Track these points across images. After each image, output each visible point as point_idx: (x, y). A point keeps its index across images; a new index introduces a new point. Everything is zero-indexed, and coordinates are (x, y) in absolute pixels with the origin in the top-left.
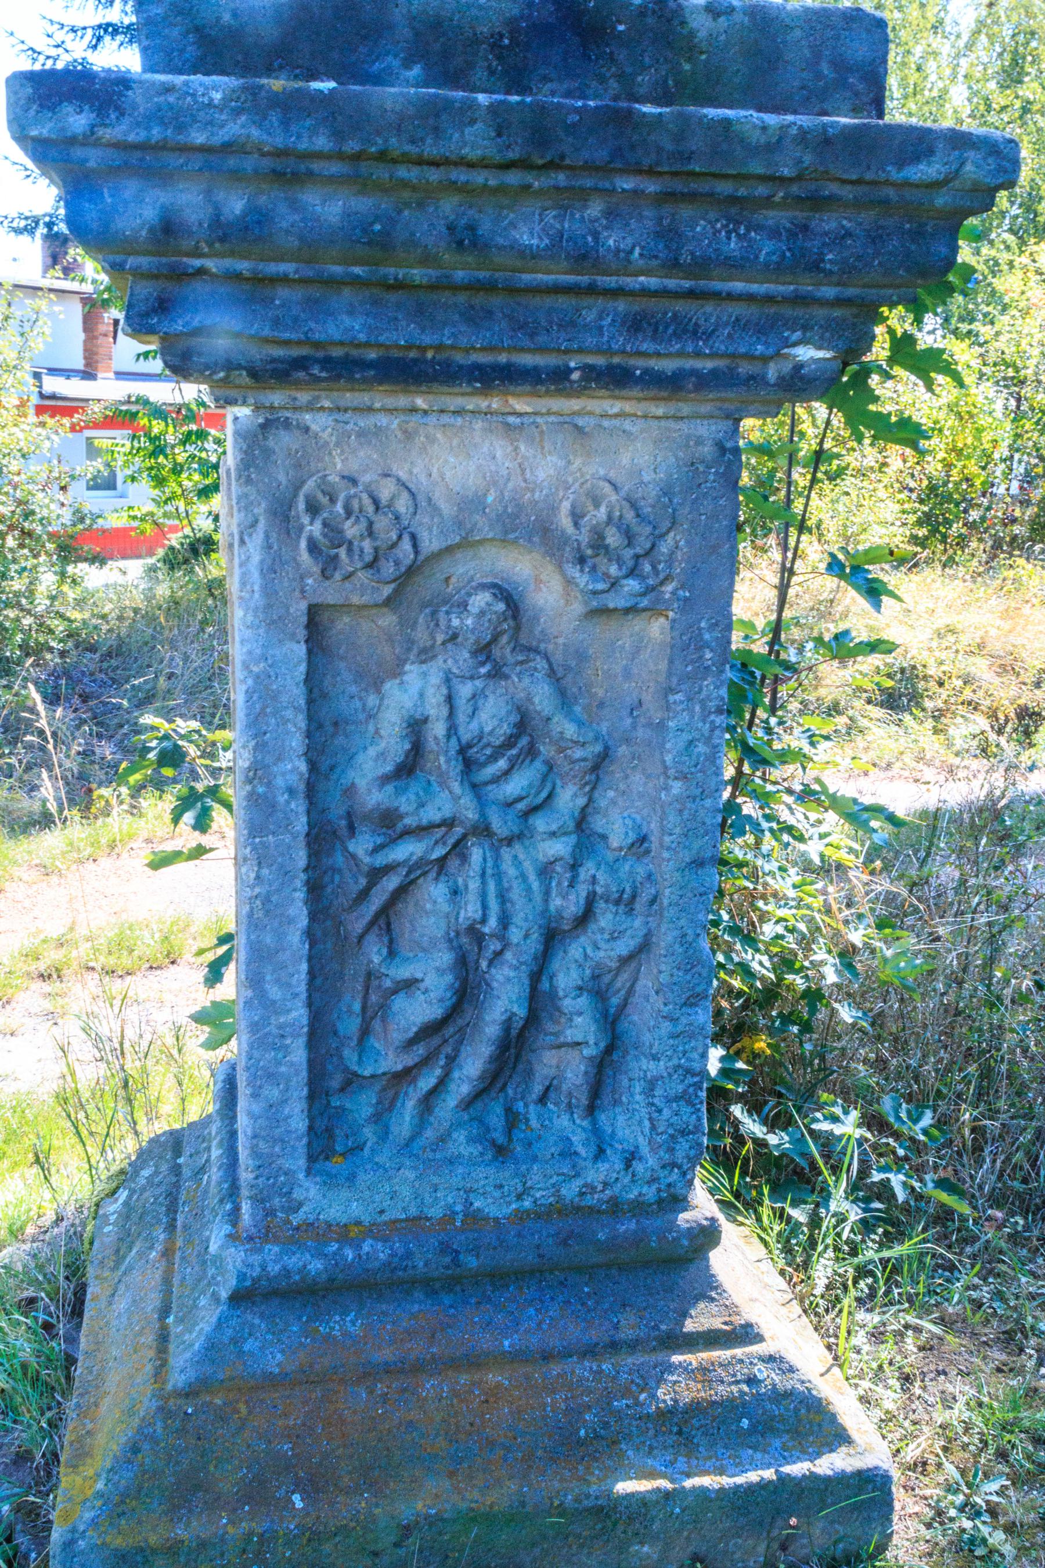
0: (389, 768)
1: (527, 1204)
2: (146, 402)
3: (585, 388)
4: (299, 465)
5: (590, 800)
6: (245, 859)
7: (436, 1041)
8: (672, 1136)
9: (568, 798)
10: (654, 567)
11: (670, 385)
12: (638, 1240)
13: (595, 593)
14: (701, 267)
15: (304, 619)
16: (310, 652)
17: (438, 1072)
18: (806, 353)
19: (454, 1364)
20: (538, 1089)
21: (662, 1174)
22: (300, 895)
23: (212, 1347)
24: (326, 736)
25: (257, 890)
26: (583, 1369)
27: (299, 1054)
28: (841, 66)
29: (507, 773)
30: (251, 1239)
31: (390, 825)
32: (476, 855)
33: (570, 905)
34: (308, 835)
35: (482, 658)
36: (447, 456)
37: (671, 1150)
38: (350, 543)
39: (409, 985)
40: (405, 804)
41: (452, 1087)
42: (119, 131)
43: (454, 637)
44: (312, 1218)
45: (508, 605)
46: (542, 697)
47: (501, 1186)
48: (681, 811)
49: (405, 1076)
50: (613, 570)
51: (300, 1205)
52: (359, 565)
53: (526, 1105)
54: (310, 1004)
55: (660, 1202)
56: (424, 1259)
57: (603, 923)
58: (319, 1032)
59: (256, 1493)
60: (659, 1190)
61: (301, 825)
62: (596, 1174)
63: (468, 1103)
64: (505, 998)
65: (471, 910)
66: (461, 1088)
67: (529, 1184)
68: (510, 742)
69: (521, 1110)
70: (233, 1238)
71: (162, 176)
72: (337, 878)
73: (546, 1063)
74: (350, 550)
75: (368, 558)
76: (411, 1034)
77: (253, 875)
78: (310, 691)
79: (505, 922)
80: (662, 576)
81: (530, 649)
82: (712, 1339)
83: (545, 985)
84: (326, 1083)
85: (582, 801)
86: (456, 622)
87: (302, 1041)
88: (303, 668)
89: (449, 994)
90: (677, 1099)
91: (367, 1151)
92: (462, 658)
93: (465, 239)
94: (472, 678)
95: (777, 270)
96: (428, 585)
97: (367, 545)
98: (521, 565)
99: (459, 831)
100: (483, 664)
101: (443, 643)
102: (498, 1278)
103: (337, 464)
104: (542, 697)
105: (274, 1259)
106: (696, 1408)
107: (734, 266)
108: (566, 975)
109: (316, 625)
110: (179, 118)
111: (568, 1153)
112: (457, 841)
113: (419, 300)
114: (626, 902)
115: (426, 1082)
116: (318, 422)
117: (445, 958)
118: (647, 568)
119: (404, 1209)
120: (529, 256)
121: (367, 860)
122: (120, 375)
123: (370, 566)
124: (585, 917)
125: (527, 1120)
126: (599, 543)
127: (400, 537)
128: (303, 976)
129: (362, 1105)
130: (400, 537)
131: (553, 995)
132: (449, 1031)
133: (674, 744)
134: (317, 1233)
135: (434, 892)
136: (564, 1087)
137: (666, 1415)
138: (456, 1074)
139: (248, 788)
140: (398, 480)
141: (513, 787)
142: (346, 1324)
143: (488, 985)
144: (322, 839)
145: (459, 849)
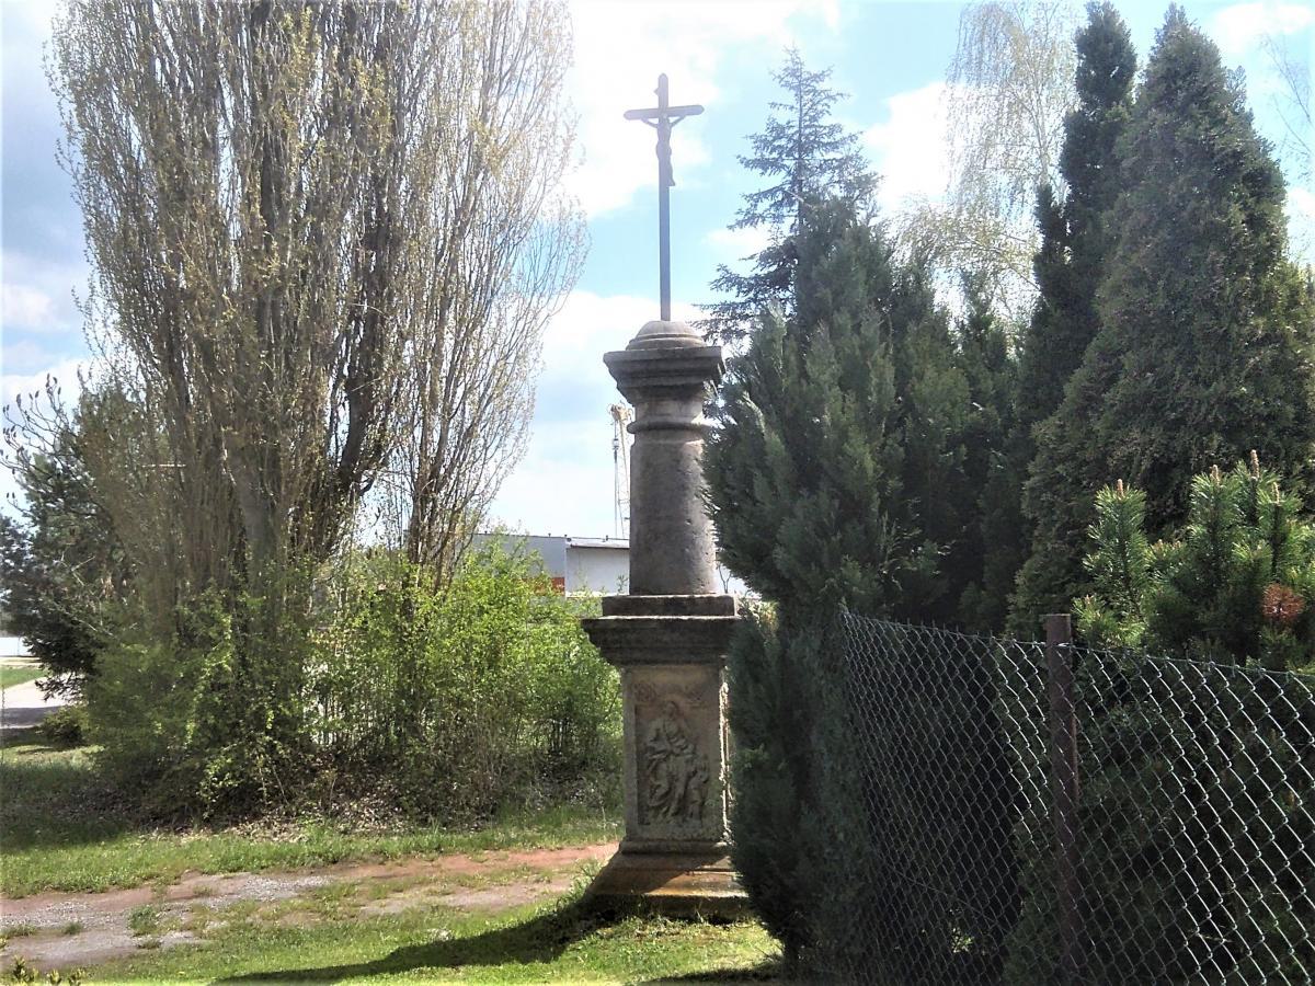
9: (691, 747)
46: (684, 726)
49: (660, 807)
124: (695, 773)
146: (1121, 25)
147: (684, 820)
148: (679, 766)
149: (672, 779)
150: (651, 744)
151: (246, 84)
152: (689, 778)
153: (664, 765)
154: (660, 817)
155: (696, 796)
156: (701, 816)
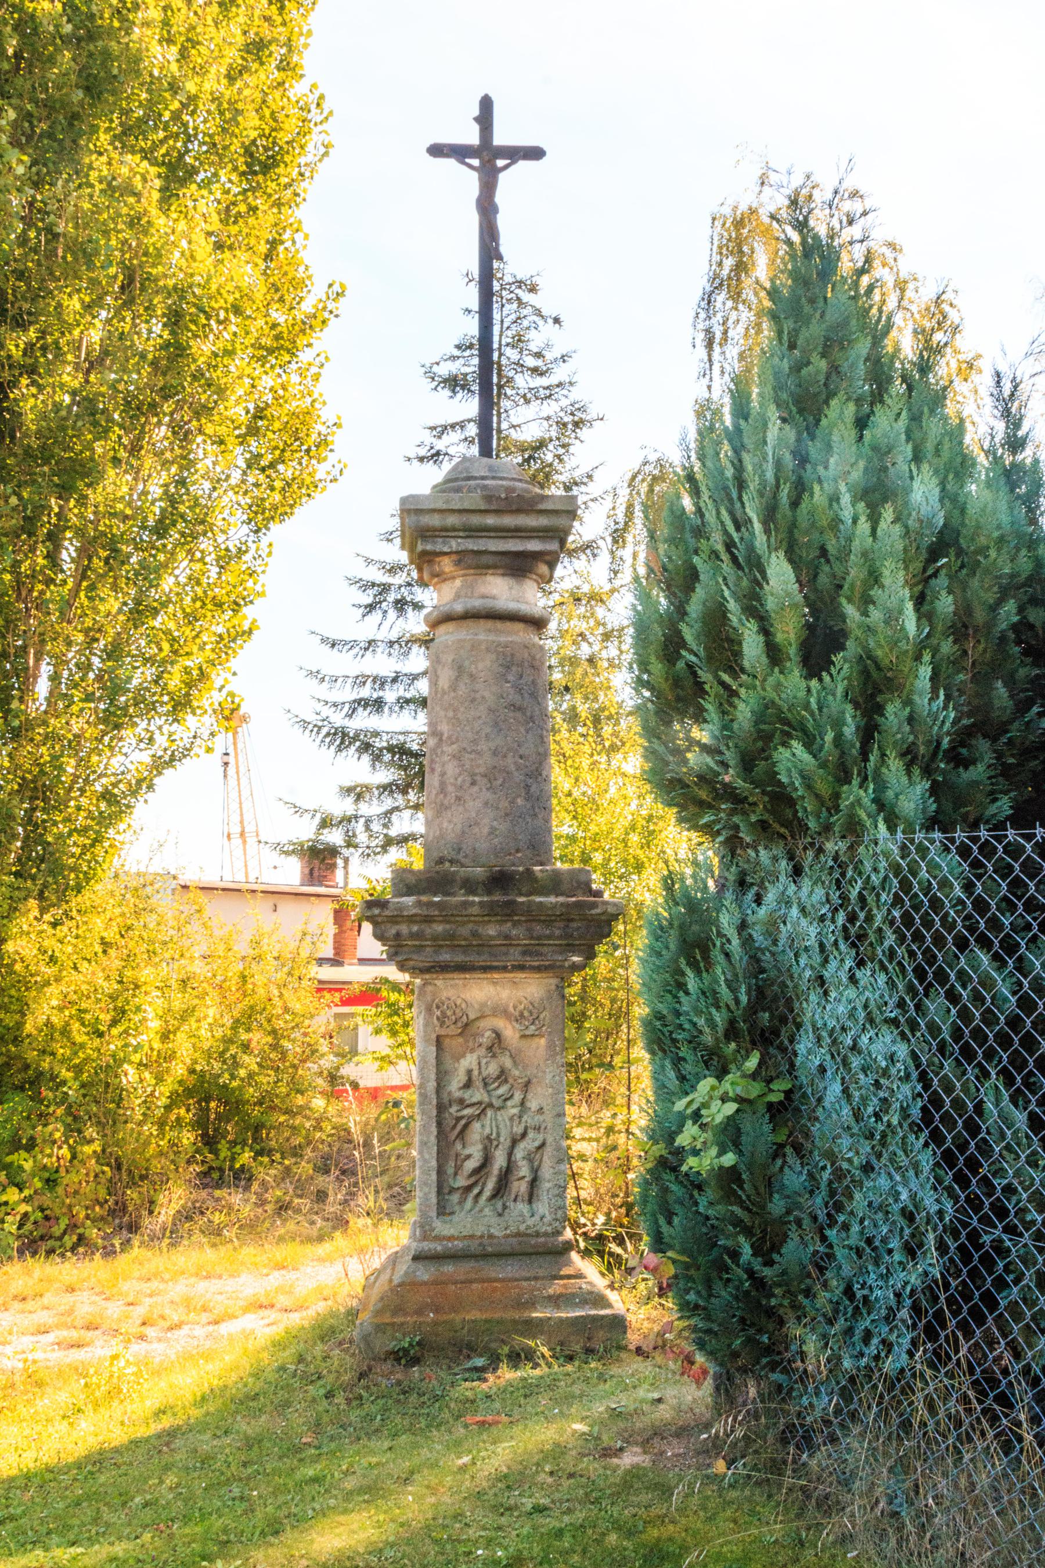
2: (387, 981)
4: (434, 994)
9: (518, 1096)
11: (538, 969)
12: (545, 1244)
14: (539, 938)
18: (575, 959)
19: (483, 1281)
23: (406, 1273)
24: (442, 1076)
26: (525, 1284)
27: (434, 1177)
28: (579, 883)
33: (518, 1130)
36: (478, 992)
39: (469, 1157)
40: (466, 1096)
42: (387, 913)
46: (508, 1063)
49: (468, 1189)
56: (474, 1246)
58: (440, 1171)
59: (419, 1312)
62: (530, 1222)
64: (500, 1161)
65: (487, 1131)
66: (487, 1193)
71: (397, 923)
79: (498, 1135)
82: (569, 1277)
92: (482, 1051)
93: (475, 934)
95: (560, 938)
96: (473, 1029)
98: (500, 1023)
102: (499, 1255)
103: (444, 995)
104: (508, 1063)
105: (427, 1246)
106: (560, 1296)
107: (549, 937)
108: (519, 1154)
109: (439, 1041)
110: (401, 908)
111: (522, 1215)
112: (484, 1108)
113: (466, 949)
114: (537, 1129)
115: (476, 1191)
116: (439, 983)
117: (480, 1147)
120: (492, 938)
122: (363, 961)
124: (524, 1135)
126: (522, 1015)
129: (455, 1198)
133: (549, 1076)
134: (438, 1238)
135: (476, 1126)
137: (550, 1297)
141: (500, 1091)
142: (449, 1268)
144: (441, 1108)
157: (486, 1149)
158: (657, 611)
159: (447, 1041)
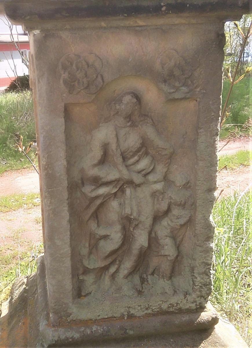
0: (96, 162)
1: (150, 311)
3: (167, 13)
5: (168, 169)
6: (46, 197)
7: (114, 257)
8: (201, 287)
9: (161, 169)
10: (192, 82)
13: (170, 93)
15: (63, 109)
16: (66, 121)
17: (116, 266)
20: (151, 270)
21: (197, 299)
22: (66, 208)
25: (51, 207)
29: (138, 161)
30: (54, 326)
31: (97, 182)
32: (128, 191)
33: (164, 206)
34: (68, 187)
35: (128, 120)
37: (200, 291)
38: (79, 80)
41: (121, 271)
43: (117, 113)
44: (74, 319)
45: (137, 99)
46: (150, 132)
47: (141, 306)
48: (203, 172)
49: (106, 268)
50: (177, 84)
51: (71, 314)
52: (82, 88)
53: (147, 276)
54: (71, 246)
55: (197, 309)
57: (150, 200)
60: (196, 305)
61: (65, 184)
63: (126, 277)
64: (141, 239)
67: (150, 304)
68: (138, 151)
69: (145, 277)
70: (48, 325)
72: (78, 201)
73: (154, 262)
74: (79, 83)
75: (85, 86)
76: (107, 255)
77: (49, 202)
78: (66, 136)
80: (195, 85)
81: (145, 115)
83: (153, 235)
84: (79, 271)
85: (165, 170)
86: (118, 107)
87: (69, 258)
88: (63, 127)
89: (120, 240)
90: (203, 273)
91: (92, 294)
92: (120, 121)
94: (124, 127)
97: (85, 80)
99: (121, 183)
100: (129, 122)
101: (114, 115)
111: (164, 293)
112: (122, 186)
114: (183, 205)
118: (190, 82)
119: (107, 315)
121: (89, 195)
123: (86, 88)
124: (167, 212)
125: (148, 281)
127: (97, 77)
128: (69, 236)
129: (89, 279)
130: (97, 77)
131: (156, 239)
132: (120, 252)
136: (161, 270)
138: (122, 266)
139: (46, 171)
140: (96, 55)
143: (133, 235)
145: (122, 190)
146: (134, 263)
147: (143, 280)
148: (140, 203)
149: (128, 224)
150: (95, 172)
151: (221, 106)
152: (157, 218)
153: (114, 204)
154: (107, 280)
155: (169, 249)
156: (174, 271)
157: (124, 229)
158: (87, 333)
159: (76, 110)
